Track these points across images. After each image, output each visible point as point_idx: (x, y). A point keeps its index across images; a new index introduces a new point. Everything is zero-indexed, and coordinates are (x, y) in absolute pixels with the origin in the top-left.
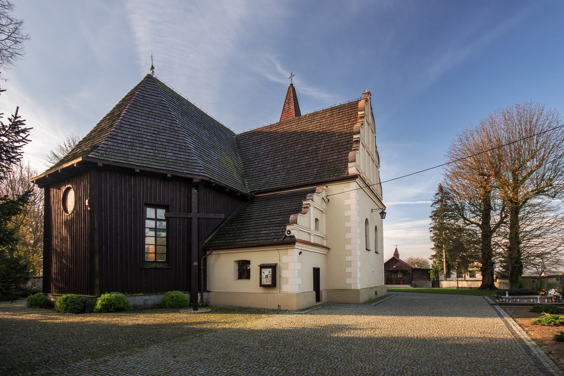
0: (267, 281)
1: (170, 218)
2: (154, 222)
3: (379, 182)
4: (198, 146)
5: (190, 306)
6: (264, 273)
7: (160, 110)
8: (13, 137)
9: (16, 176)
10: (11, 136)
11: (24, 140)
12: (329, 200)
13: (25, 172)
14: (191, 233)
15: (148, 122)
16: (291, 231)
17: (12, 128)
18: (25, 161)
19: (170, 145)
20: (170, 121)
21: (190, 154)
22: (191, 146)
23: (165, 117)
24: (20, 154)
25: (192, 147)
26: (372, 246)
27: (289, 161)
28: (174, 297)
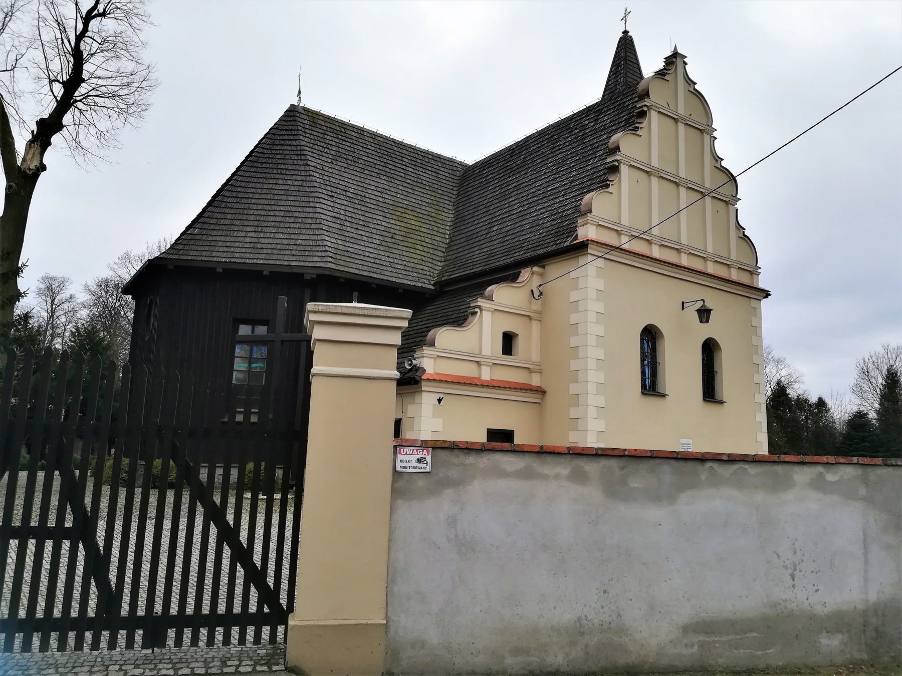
20: (303, 178)
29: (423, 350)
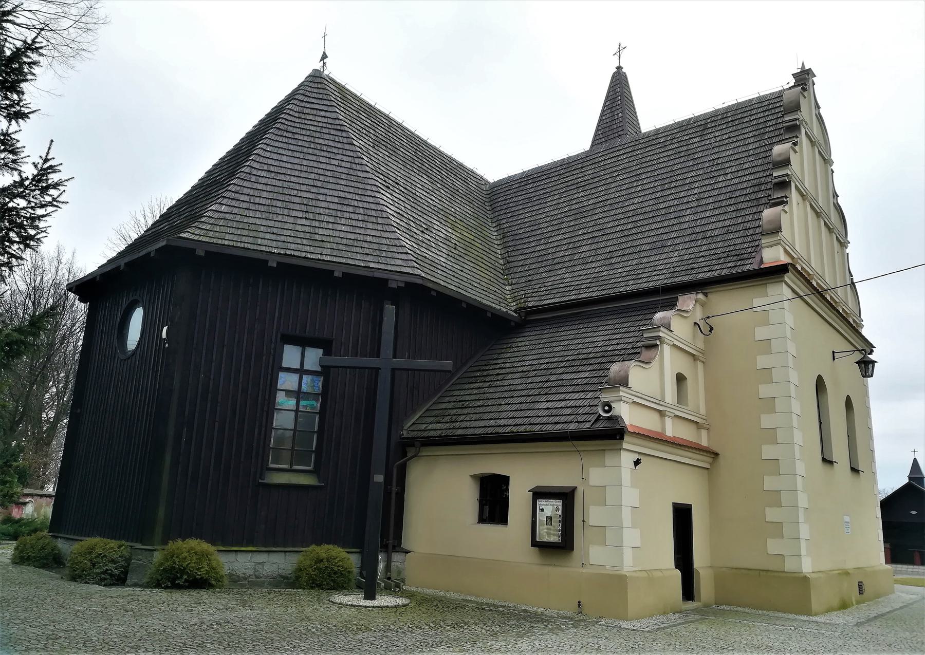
0: (550, 534)
1: (332, 369)
2: (295, 377)
3: (849, 282)
4: (403, 209)
5: (359, 587)
6: (542, 510)
7: (332, 138)
8: (36, 198)
9: (46, 278)
10: (33, 197)
11: (55, 203)
12: (711, 329)
13: (64, 270)
14: (374, 404)
15: (305, 162)
16: (613, 405)
17: (37, 181)
18: (47, 247)
19: (345, 208)
20: (350, 159)
21: (387, 228)
22: (389, 211)
23: (340, 151)
24: (43, 230)
25: (392, 212)
26: (840, 452)
27: (611, 236)
28: (321, 561)
29: (619, 391)
